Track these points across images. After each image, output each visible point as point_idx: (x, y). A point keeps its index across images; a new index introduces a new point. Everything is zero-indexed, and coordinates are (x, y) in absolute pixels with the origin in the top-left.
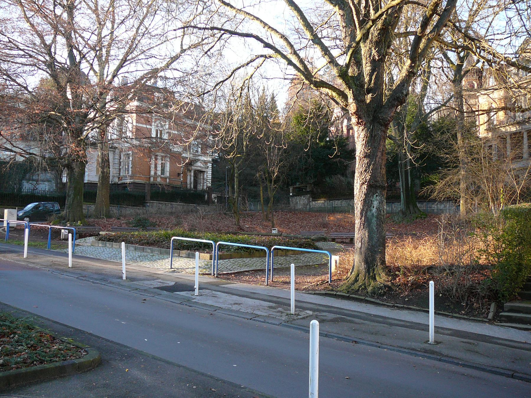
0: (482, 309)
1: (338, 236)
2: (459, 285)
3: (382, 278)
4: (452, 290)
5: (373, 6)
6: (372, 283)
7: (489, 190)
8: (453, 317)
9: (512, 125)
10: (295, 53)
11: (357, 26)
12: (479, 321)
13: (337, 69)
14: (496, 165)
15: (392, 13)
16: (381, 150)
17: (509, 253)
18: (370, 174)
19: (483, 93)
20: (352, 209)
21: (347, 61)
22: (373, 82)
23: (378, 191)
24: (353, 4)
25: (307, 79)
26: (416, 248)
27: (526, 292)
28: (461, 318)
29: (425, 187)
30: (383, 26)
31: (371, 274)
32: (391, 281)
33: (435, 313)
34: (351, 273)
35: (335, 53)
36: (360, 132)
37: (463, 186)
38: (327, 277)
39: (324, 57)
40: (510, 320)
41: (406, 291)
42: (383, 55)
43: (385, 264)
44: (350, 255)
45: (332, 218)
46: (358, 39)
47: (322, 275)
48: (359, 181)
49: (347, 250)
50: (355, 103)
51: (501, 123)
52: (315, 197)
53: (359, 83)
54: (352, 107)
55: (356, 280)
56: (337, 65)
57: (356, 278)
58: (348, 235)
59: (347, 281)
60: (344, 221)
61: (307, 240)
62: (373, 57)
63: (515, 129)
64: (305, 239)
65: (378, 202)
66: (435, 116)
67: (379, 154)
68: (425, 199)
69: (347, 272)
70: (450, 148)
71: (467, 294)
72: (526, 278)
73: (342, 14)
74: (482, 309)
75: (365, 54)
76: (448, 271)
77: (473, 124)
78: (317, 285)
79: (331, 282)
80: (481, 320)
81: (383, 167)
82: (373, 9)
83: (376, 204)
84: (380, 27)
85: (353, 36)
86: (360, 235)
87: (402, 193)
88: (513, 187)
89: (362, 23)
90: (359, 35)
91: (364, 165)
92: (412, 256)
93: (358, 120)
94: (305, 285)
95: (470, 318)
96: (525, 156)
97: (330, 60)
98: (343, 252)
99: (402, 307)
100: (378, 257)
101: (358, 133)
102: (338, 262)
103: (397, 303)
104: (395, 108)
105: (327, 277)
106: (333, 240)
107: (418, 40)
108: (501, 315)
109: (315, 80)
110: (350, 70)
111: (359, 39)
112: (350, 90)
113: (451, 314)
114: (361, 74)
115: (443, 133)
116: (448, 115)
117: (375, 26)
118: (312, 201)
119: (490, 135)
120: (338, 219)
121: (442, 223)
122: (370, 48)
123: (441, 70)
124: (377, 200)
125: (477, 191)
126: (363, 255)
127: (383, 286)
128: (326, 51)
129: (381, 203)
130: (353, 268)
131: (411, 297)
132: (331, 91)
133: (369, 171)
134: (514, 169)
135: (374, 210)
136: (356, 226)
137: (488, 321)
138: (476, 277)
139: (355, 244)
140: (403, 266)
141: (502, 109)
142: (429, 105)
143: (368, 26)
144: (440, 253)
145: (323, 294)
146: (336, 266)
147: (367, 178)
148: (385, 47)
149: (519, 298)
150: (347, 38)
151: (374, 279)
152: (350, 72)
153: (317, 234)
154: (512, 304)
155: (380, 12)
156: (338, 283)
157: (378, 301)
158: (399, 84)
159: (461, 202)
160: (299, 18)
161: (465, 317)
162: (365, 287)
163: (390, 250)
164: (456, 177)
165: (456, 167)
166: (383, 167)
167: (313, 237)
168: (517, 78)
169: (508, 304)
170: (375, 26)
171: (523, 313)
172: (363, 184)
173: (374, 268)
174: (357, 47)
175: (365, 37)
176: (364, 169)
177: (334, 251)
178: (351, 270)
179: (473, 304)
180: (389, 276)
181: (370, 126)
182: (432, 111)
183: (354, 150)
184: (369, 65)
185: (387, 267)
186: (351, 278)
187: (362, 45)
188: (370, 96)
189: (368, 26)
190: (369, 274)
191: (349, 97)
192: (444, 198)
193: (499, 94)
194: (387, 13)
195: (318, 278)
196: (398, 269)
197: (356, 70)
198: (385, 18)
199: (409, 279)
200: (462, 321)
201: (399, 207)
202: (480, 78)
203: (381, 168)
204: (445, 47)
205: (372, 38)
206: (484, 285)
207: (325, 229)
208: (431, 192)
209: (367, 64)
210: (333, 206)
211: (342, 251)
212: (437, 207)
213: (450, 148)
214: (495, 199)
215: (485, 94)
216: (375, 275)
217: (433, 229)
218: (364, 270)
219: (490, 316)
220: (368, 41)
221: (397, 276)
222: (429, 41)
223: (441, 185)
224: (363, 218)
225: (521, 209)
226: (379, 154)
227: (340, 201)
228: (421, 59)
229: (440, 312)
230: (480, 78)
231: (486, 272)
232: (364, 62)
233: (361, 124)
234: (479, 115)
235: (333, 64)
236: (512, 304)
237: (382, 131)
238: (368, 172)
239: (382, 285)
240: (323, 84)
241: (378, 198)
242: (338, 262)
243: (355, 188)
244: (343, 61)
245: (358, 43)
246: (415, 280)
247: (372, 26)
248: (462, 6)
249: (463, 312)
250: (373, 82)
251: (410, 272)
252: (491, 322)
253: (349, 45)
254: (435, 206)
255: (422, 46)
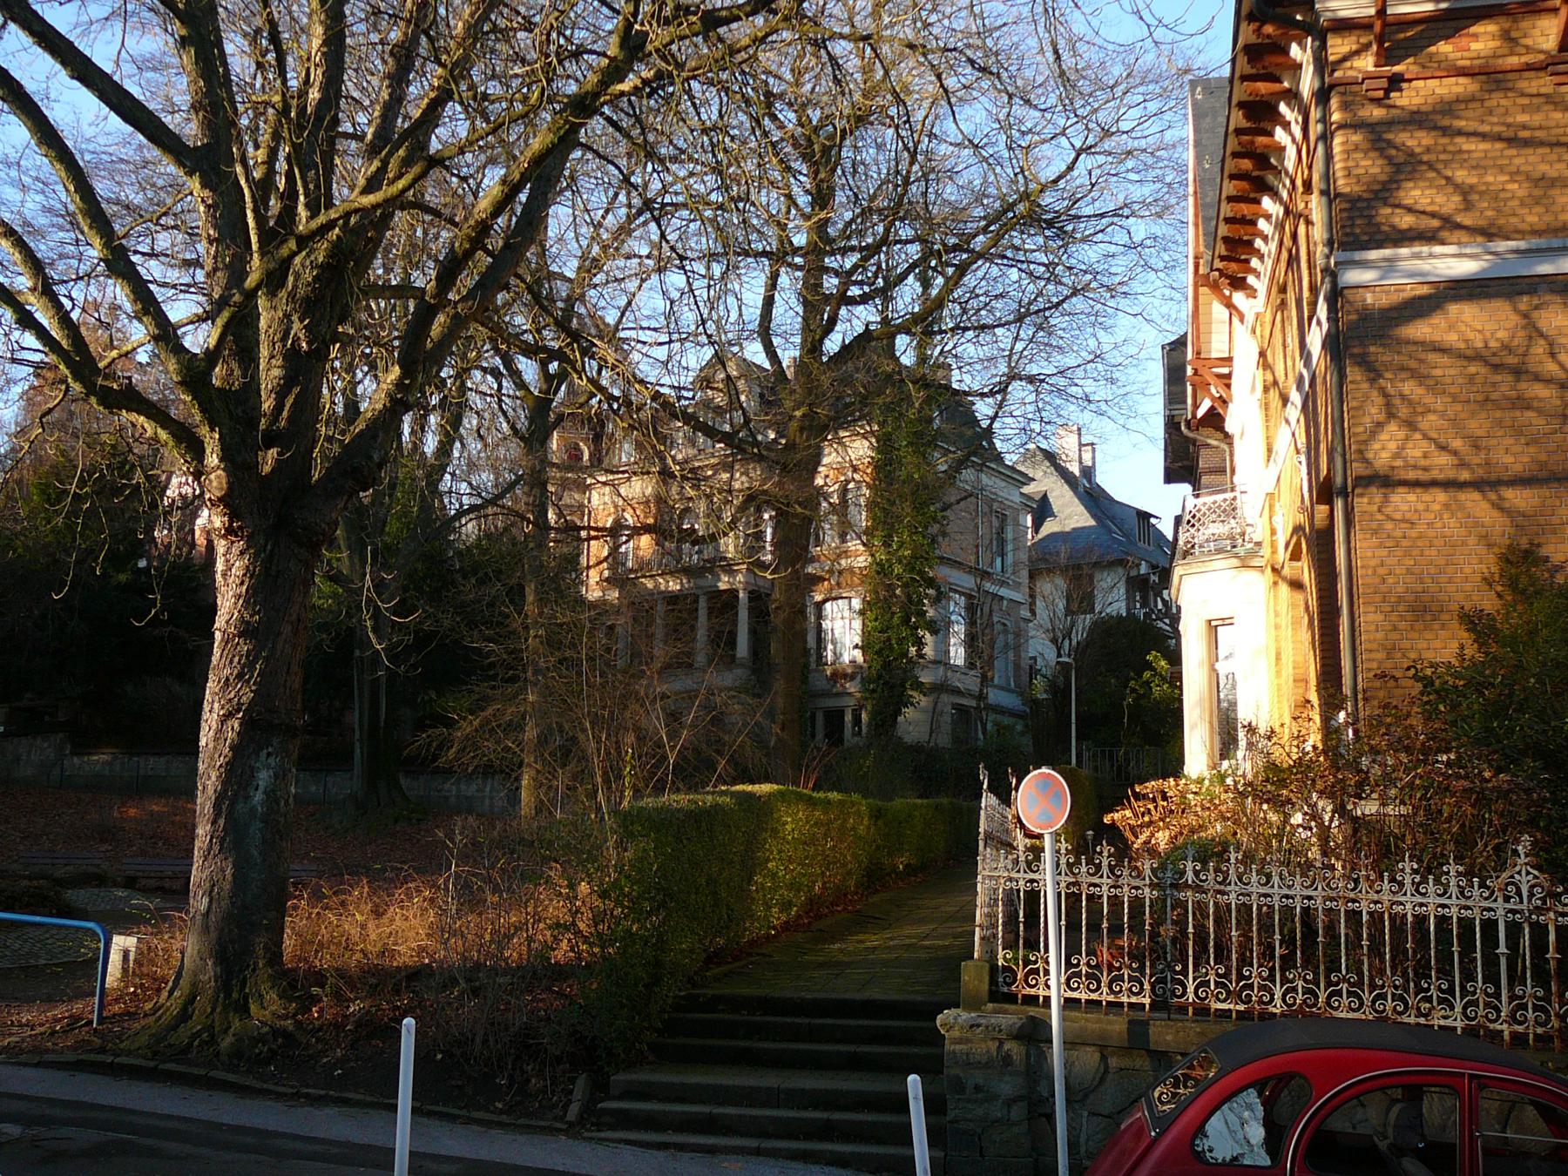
0: (553, 1092)
1: (147, 868)
2: (493, 1024)
3: (268, 1008)
4: (473, 1040)
5: (306, 196)
6: (236, 1024)
7: (599, 750)
8: (469, 1121)
9: (671, 573)
10: (47, 290)
11: (255, 247)
12: (542, 1130)
13: (178, 362)
14: (621, 683)
15: (360, 226)
16: (294, 617)
17: (629, 931)
18: (253, 688)
19: (603, 479)
20: (189, 791)
21: (212, 342)
22: (285, 414)
23: (275, 741)
24: (247, 180)
25: (77, 376)
26: (378, 913)
27: (669, 1041)
28: (493, 1122)
29: (424, 732)
30: (331, 257)
31: (235, 995)
32: (295, 1015)
33: (414, 1111)
34: (171, 993)
35: (179, 310)
36: (231, 557)
37: (531, 733)
38: (90, 1008)
39: (140, 321)
40: (625, 1121)
41: (339, 1045)
42: (324, 341)
43: (281, 963)
44: (174, 933)
45: (132, 812)
46: (250, 282)
47: (70, 1000)
48: (216, 705)
49: (165, 918)
50: (224, 470)
51: (643, 566)
52: (83, 742)
53: (243, 411)
54: (217, 481)
55: (184, 1015)
56: (178, 349)
57: (184, 1009)
58: (178, 868)
59: (154, 1018)
60: (173, 822)
61: (35, 883)
62: (293, 342)
63: (678, 587)
64: (29, 878)
65: (271, 772)
66: (470, 528)
67: (287, 630)
68: (424, 764)
69: (159, 990)
70: (499, 624)
71: (512, 1051)
72: (670, 1001)
73: (210, 202)
74: (553, 1092)
75: (271, 331)
76: (463, 985)
77: (571, 563)
78: (53, 1033)
79: (98, 1024)
80: (544, 1128)
81: (295, 668)
82: (307, 206)
83: (264, 777)
84: (321, 259)
85: (237, 272)
86: (207, 872)
87: (357, 744)
88: (660, 745)
89: (270, 238)
90: (256, 266)
91: (236, 659)
92: (364, 938)
93: (231, 522)
94: (11, 1035)
95: (519, 1122)
96: (700, 659)
97: (157, 332)
98: (153, 926)
99: (320, 1098)
100: (260, 943)
101: (228, 561)
102: (132, 957)
103: (307, 1086)
104: (345, 498)
105: (90, 1008)
106: (130, 883)
107: (426, 314)
108: (601, 1109)
109: (105, 383)
110: (217, 369)
111: (253, 285)
112: (212, 430)
113: (463, 1112)
114: (251, 387)
115: (482, 582)
116: (505, 529)
117: (308, 255)
118: (73, 754)
119: (614, 595)
120: (152, 813)
121: (454, 844)
122: (287, 316)
123: (494, 402)
124: (268, 767)
125: (568, 752)
126: (214, 935)
127: (267, 1033)
128: (148, 305)
129: (280, 776)
130: (179, 975)
131: (352, 1064)
132: (154, 425)
133: (250, 678)
134: (664, 696)
135: (258, 797)
136: (197, 844)
137: (564, 1127)
138: (541, 1000)
139: (191, 902)
140: (337, 969)
141: (647, 529)
142: (457, 491)
143: (284, 252)
144: (440, 931)
145: (67, 1063)
146: (125, 970)
147: (244, 698)
148: (332, 317)
149: (651, 1058)
150: (219, 274)
151: (244, 1010)
152: (218, 375)
153: (79, 862)
154: (634, 1077)
155: (321, 219)
156: (126, 1025)
157: (250, 1081)
158: (362, 430)
159: (524, 782)
160: (72, 188)
161: (504, 1118)
162: (212, 1036)
163: (301, 919)
164: (513, 709)
165: (513, 679)
166: (295, 668)
167: (59, 873)
168: (692, 452)
169: (620, 1078)
170: (308, 255)
171: (659, 1100)
172: (229, 716)
173: (245, 978)
174: (246, 306)
175: (274, 280)
176: (236, 672)
177: (125, 923)
178: (170, 984)
179: (528, 1081)
180: (290, 1002)
181: (266, 545)
182: (461, 513)
183: (213, 610)
184: (280, 362)
185: (286, 973)
186: (168, 1009)
187: (262, 302)
188: (273, 453)
189: (284, 252)
190: (228, 995)
191: (208, 451)
192: (476, 767)
193: (639, 488)
194: (346, 223)
195: (59, 1011)
196: (319, 978)
197: (237, 372)
198: (338, 236)
199: (351, 1010)
200: (493, 1132)
201: (344, 785)
202: (597, 438)
203: (288, 673)
204: (508, 343)
205: (295, 286)
206: (560, 1024)
207: (106, 847)
208: (440, 747)
209: (274, 361)
210: (142, 772)
211: (147, 922)
212: (459, 790)
213: (499, 624)
214: (613, 774)
215: (604, 484)
216: (246, 998)
217: (429, 863)
218: (213, 983)
219: (574, 1111)
220: (283, 294)
221: (316, 1000)
222: (458, 323)
223: (468, 730)
224: (222, 822)
225: (668, 810)
226: (287, 630)
227: (163, 760)
228: (431, 368)
229: (433, 1108)
230: (597, 438)
231: (570, 986)
232: (264, 352)
233: (236, 536)
234: (589, 539)
235: (167, 345)
236: (634, 1077)
237: (300, 561)
238: (248, 681)
239: (266, 1029)
240: (130, 398)
241: (271, 761)
242: (132, 957)
243: (204, 728)
244: (198, 340)
245: (251, 295)
246: (369, 1011)
247: (295, 254)
248: (561, 240)
249: (500, 1105)
250: (285, 414)
251: (353, 988)
252: (573, 1130)
253: (221, 296)
254: (450, 787)
255: (436, 329)
